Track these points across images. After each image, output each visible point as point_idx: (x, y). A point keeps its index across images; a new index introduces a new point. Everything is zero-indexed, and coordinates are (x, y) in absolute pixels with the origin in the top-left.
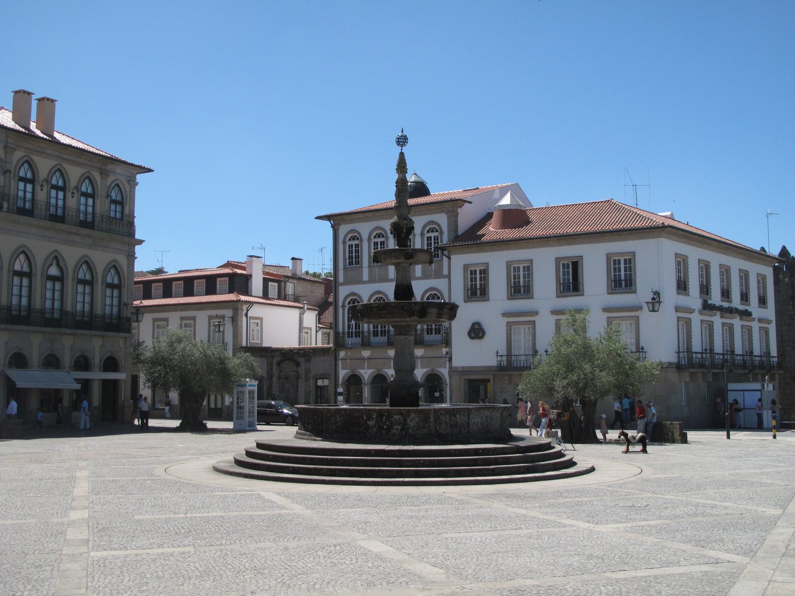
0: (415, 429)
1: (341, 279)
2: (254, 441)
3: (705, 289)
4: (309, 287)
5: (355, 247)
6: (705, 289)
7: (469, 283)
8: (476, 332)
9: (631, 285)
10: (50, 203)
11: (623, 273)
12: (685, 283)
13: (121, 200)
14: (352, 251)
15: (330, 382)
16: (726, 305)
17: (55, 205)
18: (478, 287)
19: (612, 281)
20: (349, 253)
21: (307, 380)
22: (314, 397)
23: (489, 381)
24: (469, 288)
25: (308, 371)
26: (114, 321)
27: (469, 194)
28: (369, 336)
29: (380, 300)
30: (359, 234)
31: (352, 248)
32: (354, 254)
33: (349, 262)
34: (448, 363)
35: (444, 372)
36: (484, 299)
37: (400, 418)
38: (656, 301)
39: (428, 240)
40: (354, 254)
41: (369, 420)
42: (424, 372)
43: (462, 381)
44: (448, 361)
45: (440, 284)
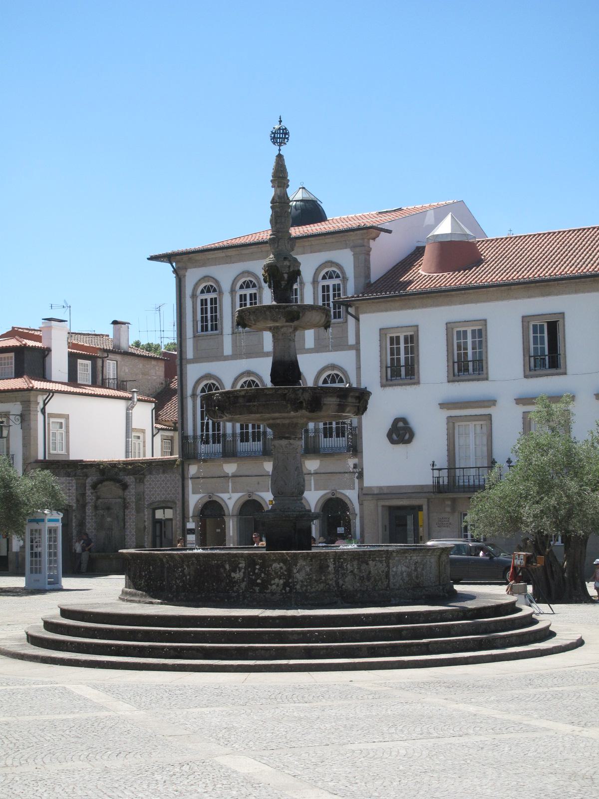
0: (305, 583)
1: (190, 354)
5: (211, 304)
7: (389, 357)
11: (402, 356)
15: (175, 514)
18: (403, 362)
20: (202, 313)
21: (139, 510)
23: (420, 508)
24: (456, 360)
25: (140, 497)
28: (234, 441)
30: (217, 282)
32: (209, 315)
33: (202, 326)
34: (356, 481)
35: (351, 495)
37: (281, 568)
39: (323, 291)
40: (209, 315)
41: (235, 571)
43: (380, 509)
44: (357, 478)
45: (344, 359)
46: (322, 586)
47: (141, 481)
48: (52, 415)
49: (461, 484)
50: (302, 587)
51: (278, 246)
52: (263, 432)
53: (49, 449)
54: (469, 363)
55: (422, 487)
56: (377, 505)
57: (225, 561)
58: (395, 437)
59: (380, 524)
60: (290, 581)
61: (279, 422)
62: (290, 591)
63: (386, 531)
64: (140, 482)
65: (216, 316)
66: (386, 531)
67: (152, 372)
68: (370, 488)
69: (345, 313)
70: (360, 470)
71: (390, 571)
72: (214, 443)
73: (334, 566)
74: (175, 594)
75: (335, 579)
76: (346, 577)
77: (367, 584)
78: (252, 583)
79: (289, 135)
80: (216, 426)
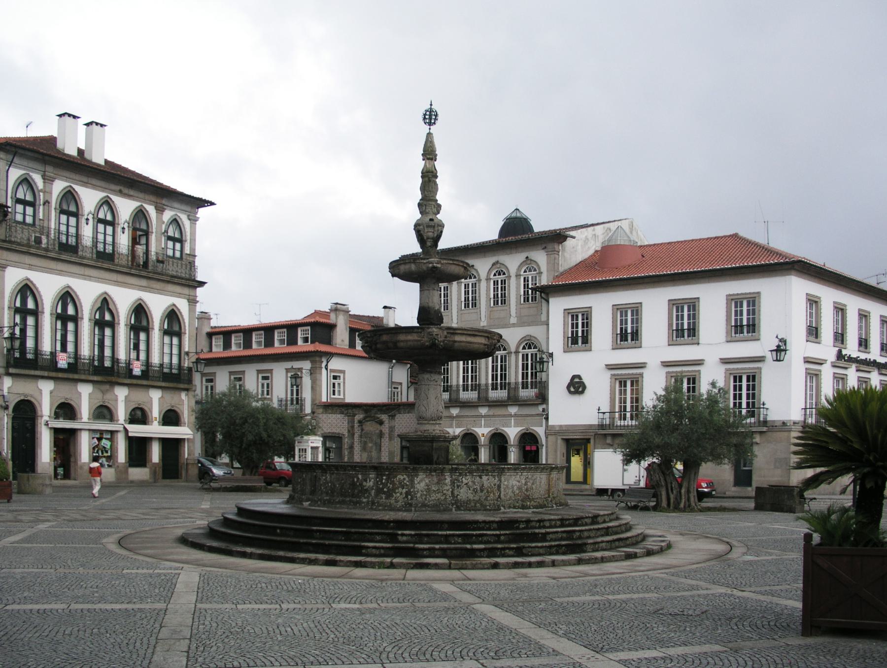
0: (425, 493)
2: (234, 506)
3: (840, 337)
6: (840, 337)
8: (576, 386)
10: (97, 239)
12: (817, 329)
13: (180, 237)
14: (502, 290)
16: (863, 356)
17: (111, 243)
18: (580, 334)
21: (391, 438)
24: (570, 336)
25: (392, 429)
26: (174, 371)
28: (458, 391)
31: (497, 285)
34: (544, 421)
35: (540, 431)
37: (404, 479)
38: (780, 350)
41: (366, 481)
44: (545, 418)
46: (439, 495)
47: (392, 417)
48: (332, 371)
53: (330, 394)
55: (591, 425)
58: (572, 389)
60: (412, 490)
62: (412, 499)
68: (553, 426)
69: (540, 297)
72: (501, 389)
75: (451, 490)
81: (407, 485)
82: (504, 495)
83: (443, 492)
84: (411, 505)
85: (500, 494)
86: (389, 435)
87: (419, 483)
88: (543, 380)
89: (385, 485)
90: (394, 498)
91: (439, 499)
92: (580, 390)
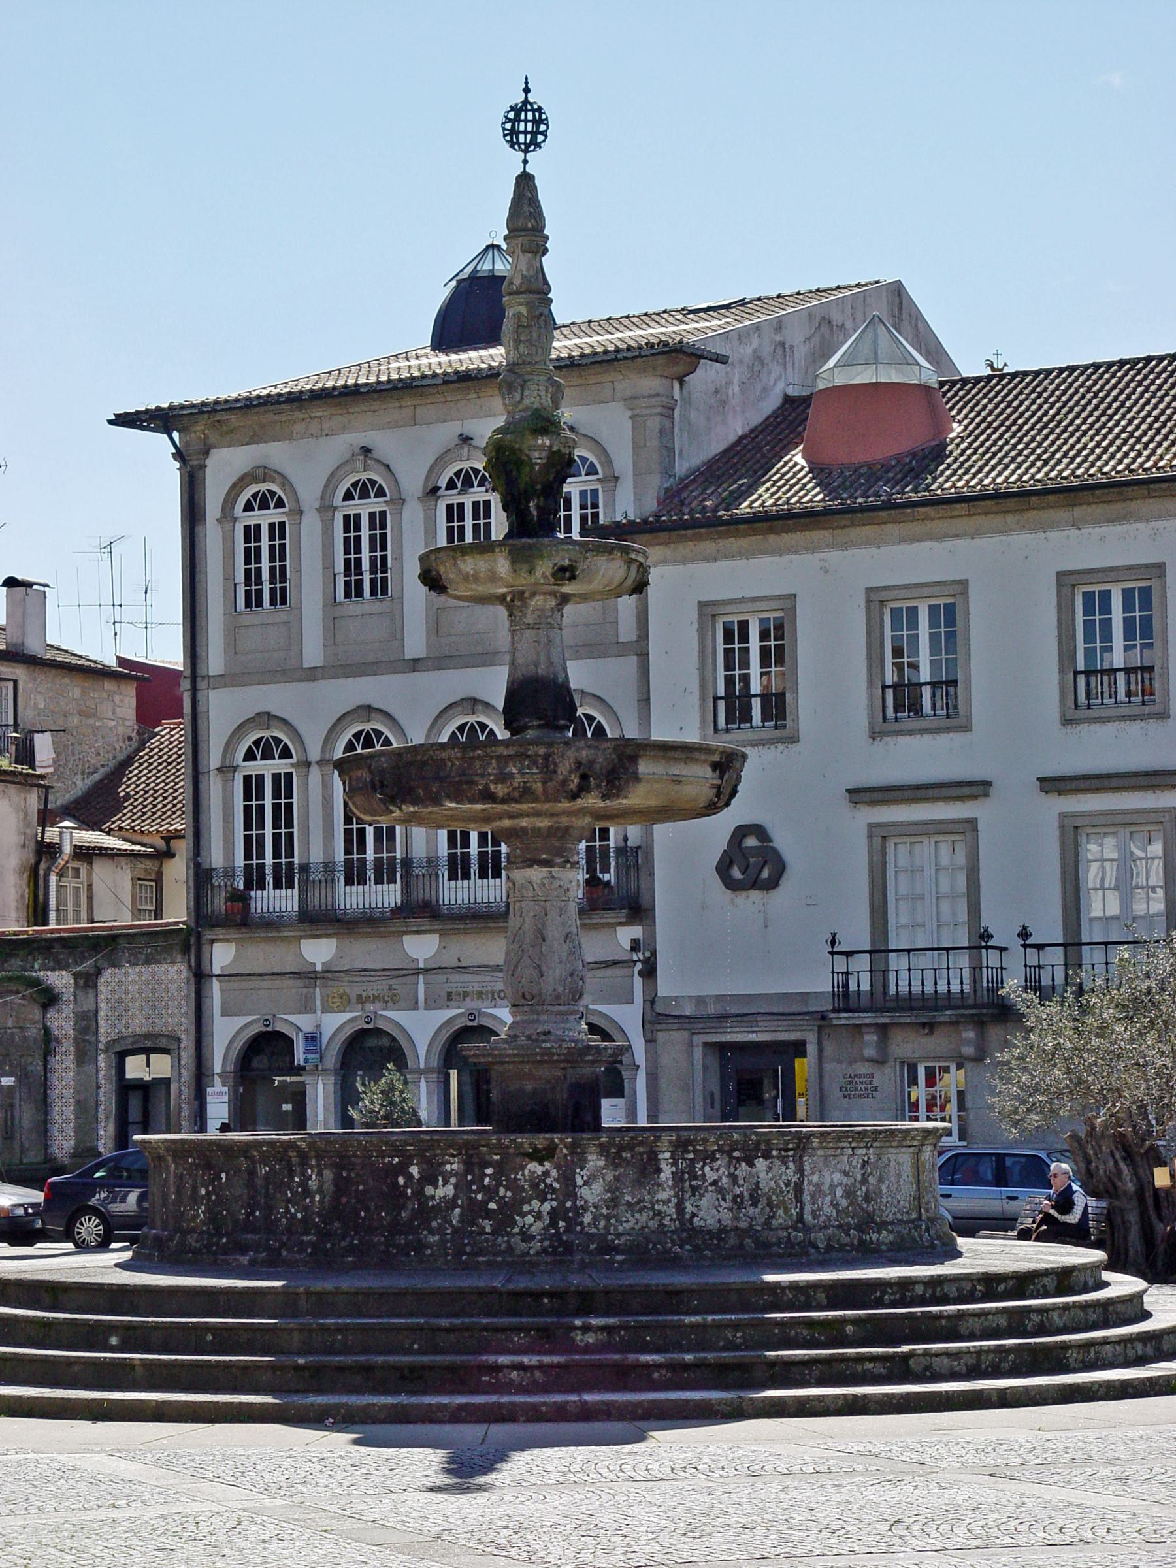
0: (605, 1211)
1: (215, 661)
4: (77, 692)
5: (272, 537)
7: (721, 673)
9: (781, 714)
15: (177, 1064)
19: (884, 687)
20: (247, 561)
21: (84, 1054)
22: (111, 1128)
23: (799, 1049)
24: (721, 692)
25: (87, 1022)
27: (714, 324)
29: (368, 743)
30: (285, 482)
33: (248, 594)
34: (638, 982)
36: (1147, 709)
37: (546, 1174)
42: (416, 1038)
43: (698, 1052)
44: (640, 973)
46: (643, 1217)
47: (87, 982)
49: (904, 988)
50: (595, 1219)
51: (522, 398)
52: (402, 860)
54: (753, 700)
56: (691, 1045)
57: (411, 1157)
58: (736, 873)
59: (699, 1091)
60: (569, 1204)
61: (524, 824)
62: (568, 1230)
63: (712, 1106)
64: (86, 986)
65: (283, 568)
66: (712, 1106)
67: (105, 709)
70: (648, 954)
71: (806, 1183)
73: (674, 1169)
74: (285, 1238)
75: (674, 1200)
76: (702, 1195)
77: (751, 1210)
78: (475, 1211)
79: (547, 125)
80: (385, 837)
81: (554, 1190)
82: (813, 1212)
83: (653, 1208)
84: (569, 1248)
85: (802, 1209)
86: (76, 1042)
87: (586, 1183)
88: (629, 844)
89: (491, 1192)
90: (516, 1230)
91: (643, 1228)
92: (765, 874)
